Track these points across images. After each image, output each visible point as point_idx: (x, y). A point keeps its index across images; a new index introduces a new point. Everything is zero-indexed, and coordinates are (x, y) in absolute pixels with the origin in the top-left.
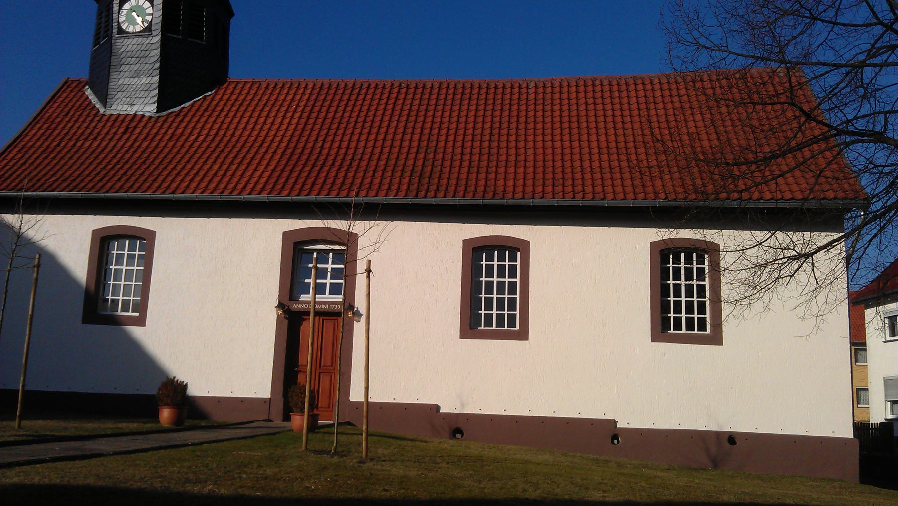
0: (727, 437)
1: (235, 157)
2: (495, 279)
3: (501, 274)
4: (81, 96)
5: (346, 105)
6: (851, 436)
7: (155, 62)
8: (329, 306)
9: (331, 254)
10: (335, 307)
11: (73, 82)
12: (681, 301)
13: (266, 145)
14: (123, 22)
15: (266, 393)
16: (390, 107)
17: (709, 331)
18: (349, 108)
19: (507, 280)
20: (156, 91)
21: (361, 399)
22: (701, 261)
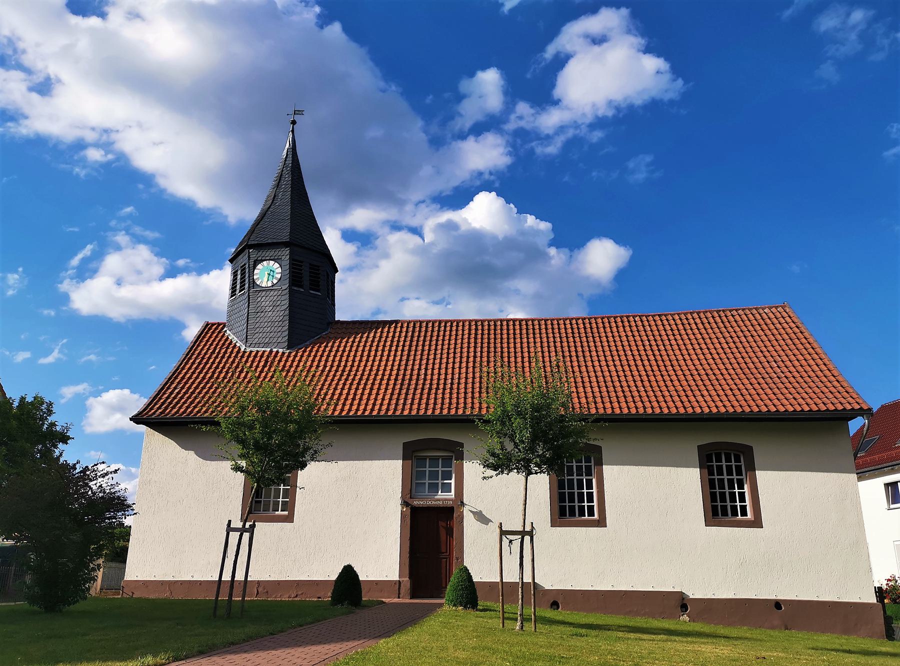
0: (773, 604)
1: (330, 385)
2: (575, 477)
3: (730, 473)
4: (223, 336)
5: (431, 341)
6: (875, 601)
7: (285, 310)
8: (443, 503)
9: (428, 460)
10: (448, 502)
11: (213, 324)
12: (586, 490)
13: (380, 373)
14: (256, 279)
15: (395, 577)
16: (472, 340)
17: (596, 516)
18: (401, 344)
19: (716, 477)
20: (287, 333)
21: (530, 580)
22: (738, 460)
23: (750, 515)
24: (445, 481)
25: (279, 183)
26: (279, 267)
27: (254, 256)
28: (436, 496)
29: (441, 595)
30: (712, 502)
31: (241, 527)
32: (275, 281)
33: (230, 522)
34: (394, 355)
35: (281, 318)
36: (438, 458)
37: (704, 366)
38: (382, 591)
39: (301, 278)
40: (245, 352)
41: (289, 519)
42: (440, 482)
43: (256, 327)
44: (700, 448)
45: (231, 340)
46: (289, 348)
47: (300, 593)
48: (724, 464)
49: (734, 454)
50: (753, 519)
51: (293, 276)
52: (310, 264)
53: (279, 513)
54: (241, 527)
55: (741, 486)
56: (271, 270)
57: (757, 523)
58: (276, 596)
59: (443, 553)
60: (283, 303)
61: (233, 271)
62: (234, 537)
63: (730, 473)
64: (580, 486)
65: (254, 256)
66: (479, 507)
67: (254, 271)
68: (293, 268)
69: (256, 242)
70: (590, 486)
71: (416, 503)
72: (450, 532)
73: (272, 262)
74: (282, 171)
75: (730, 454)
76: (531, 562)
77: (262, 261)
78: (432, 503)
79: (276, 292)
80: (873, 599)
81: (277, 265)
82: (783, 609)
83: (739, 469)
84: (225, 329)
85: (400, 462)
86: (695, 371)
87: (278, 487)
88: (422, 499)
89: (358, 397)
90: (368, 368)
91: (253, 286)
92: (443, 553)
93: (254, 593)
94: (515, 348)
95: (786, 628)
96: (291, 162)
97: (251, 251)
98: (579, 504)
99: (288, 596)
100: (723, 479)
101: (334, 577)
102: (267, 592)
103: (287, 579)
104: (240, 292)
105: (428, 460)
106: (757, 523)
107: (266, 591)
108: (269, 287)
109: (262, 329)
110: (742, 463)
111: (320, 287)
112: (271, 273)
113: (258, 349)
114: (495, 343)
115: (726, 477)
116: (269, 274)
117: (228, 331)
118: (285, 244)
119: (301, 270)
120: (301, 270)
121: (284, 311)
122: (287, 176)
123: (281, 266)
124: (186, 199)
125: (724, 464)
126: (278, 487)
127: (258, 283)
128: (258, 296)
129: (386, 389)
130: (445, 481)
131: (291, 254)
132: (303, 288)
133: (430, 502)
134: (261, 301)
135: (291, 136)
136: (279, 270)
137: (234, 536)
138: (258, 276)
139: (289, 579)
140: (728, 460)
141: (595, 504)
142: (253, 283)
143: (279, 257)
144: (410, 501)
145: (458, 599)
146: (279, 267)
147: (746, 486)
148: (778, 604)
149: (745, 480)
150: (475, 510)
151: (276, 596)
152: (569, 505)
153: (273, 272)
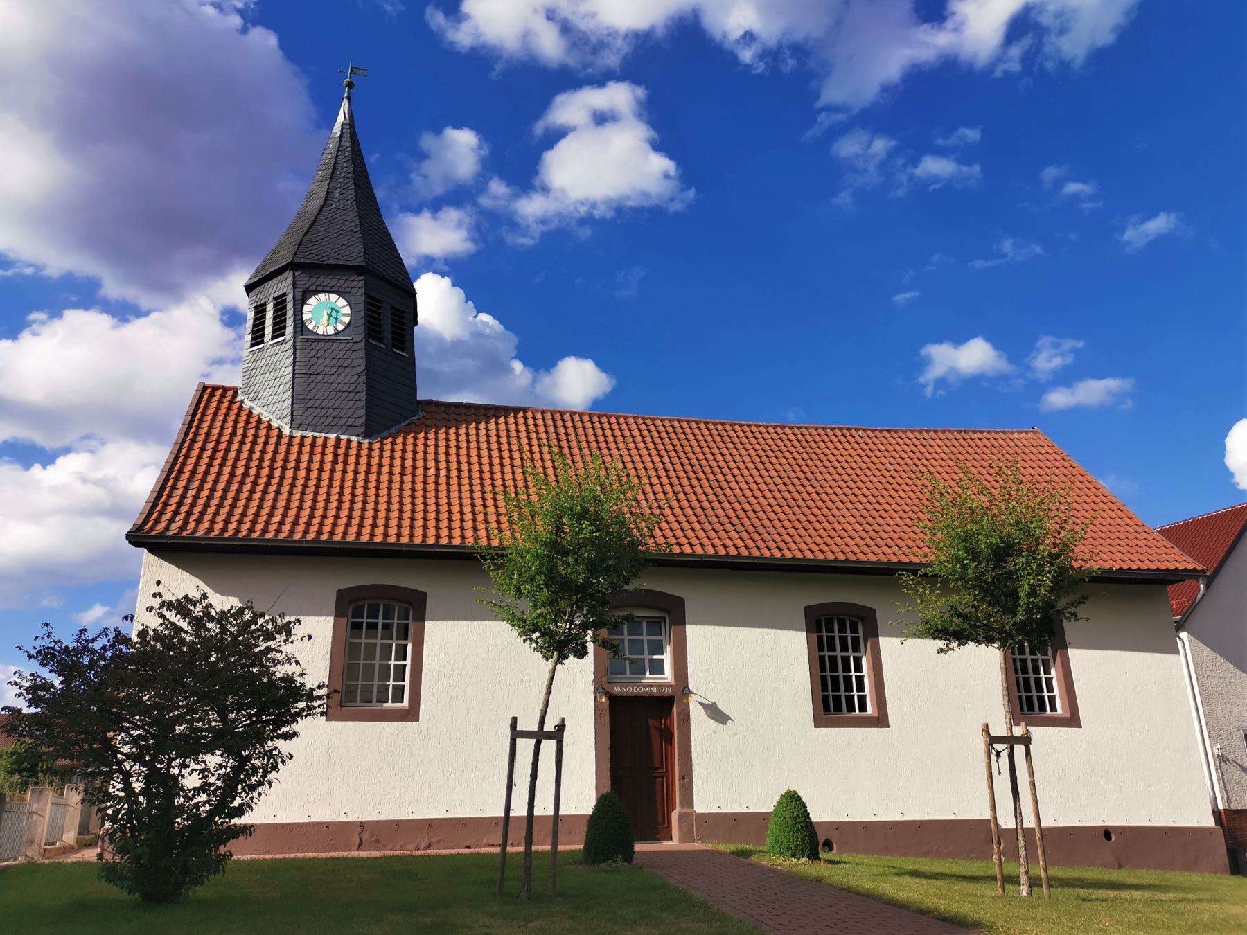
3: (844, 648)
7: (359, 374)
9: (644, 624)
14: (308, 320)
22: (854, 629)
23: (870, 710)
24: (655, 657)
25: (333, 173)
26: (346, 306)
27: (303, 283)
28: (643, 679)
29: (658, 836)
30: (823, 691)
31: (536, 730)
32: (340, 327)
33: (514, 720)
34: (197, 456)
35: (353, 387)
36: (659, 620)
37: (702, 504)
38: (570, 833)
39: (380, 326)
40: (291, 437)
41: (412, 714)
42: (646, 657)
43: (309, 397)
44: (808, 610)
45: (259, 416)
46: (366, 437)
47: (434, 840)
48: (837, 634)
49: (850, 620)
50: (877, 715)
51: (369, 322)
52: (392, 308)
53: (389, 705)
54: (536, 730)
55: (1047, 671)
56: (333, 309)
57: (881, 720)
58: (394, 847)
59: (658, 768)
60: (355, 363)
61: (255, 305)
62: (525, 747)
63: (844, 648)
64: (847, 668)
65: (303, 283)
66: (712, 698)
67: (302, 308)
68: (369, 310)
69: (308, 261)
70: (402, 655)
71: (617, 690)
72: (667, 736)
73: (334, 297)
74: (337, 156)
75: (844, 619)
76: (528, 779)
77: (317, 292)
78: (641, 689)
79: (342, 346)
80: (1211, 823)
81: (342, 302)
82: (1113, 839)
83: (855, 641)
84: (239, 398)
85: (331, 620)
86: (696, 502)
87: (386, 662)
88: (623, 684)
89: (356, 521)
90: (225, 478)
91: (302, 331)
92: (658, 768)
93: (355, 844)
94: (392, 458)
95: (1120, 867)
96: (349, 144)
97: (297, 273)
98: (380, 683)
99: (414, 846)
100: (836, 657)
101: (590, 812)
102: (377, 841)
103: (411, 817)
104: (273, 338)
105: (644, 624)
106: (881, 720)
107: (374, 839)
108: (330, 335)
109: (319, 402)
110: (861, 634)
111: (406, 345)
112: (333, 314)
113: (316, 434)
114: (436, 453)
115: (839, 654)
116: (330, 315)
117: (246, 401)
118: (357, 270)
119: (380, 314)
120: (380, 314)
121: (357, 377)
122: (345, 165)
123: (350, 304)
124: (538, 168)
125: (837, 634)
126: (386, 662)
127: (310, 327)
128: (311, 348)
129: (260, 507)
130: (655, 657)
131: (366, 286)
132: (383, 344)
133: (638, 689)
134: (317, 356)
135: (347, 106)
136: (347, 310)
137: (525, 747)
138: (310, 316)
139: (414, 818)
140: (842, 630)
141: (407, 683)
142: (300, 326)
143: (348, 290)
144: (607, 687)
145: (797, 845)
146: (346, 306)
147: (1053, 671)
148: (1107, 833)
149: (1051, 662)
150: (706, 702)
151: (394, 847)
152: (833, 696)
153: (337, 312)
